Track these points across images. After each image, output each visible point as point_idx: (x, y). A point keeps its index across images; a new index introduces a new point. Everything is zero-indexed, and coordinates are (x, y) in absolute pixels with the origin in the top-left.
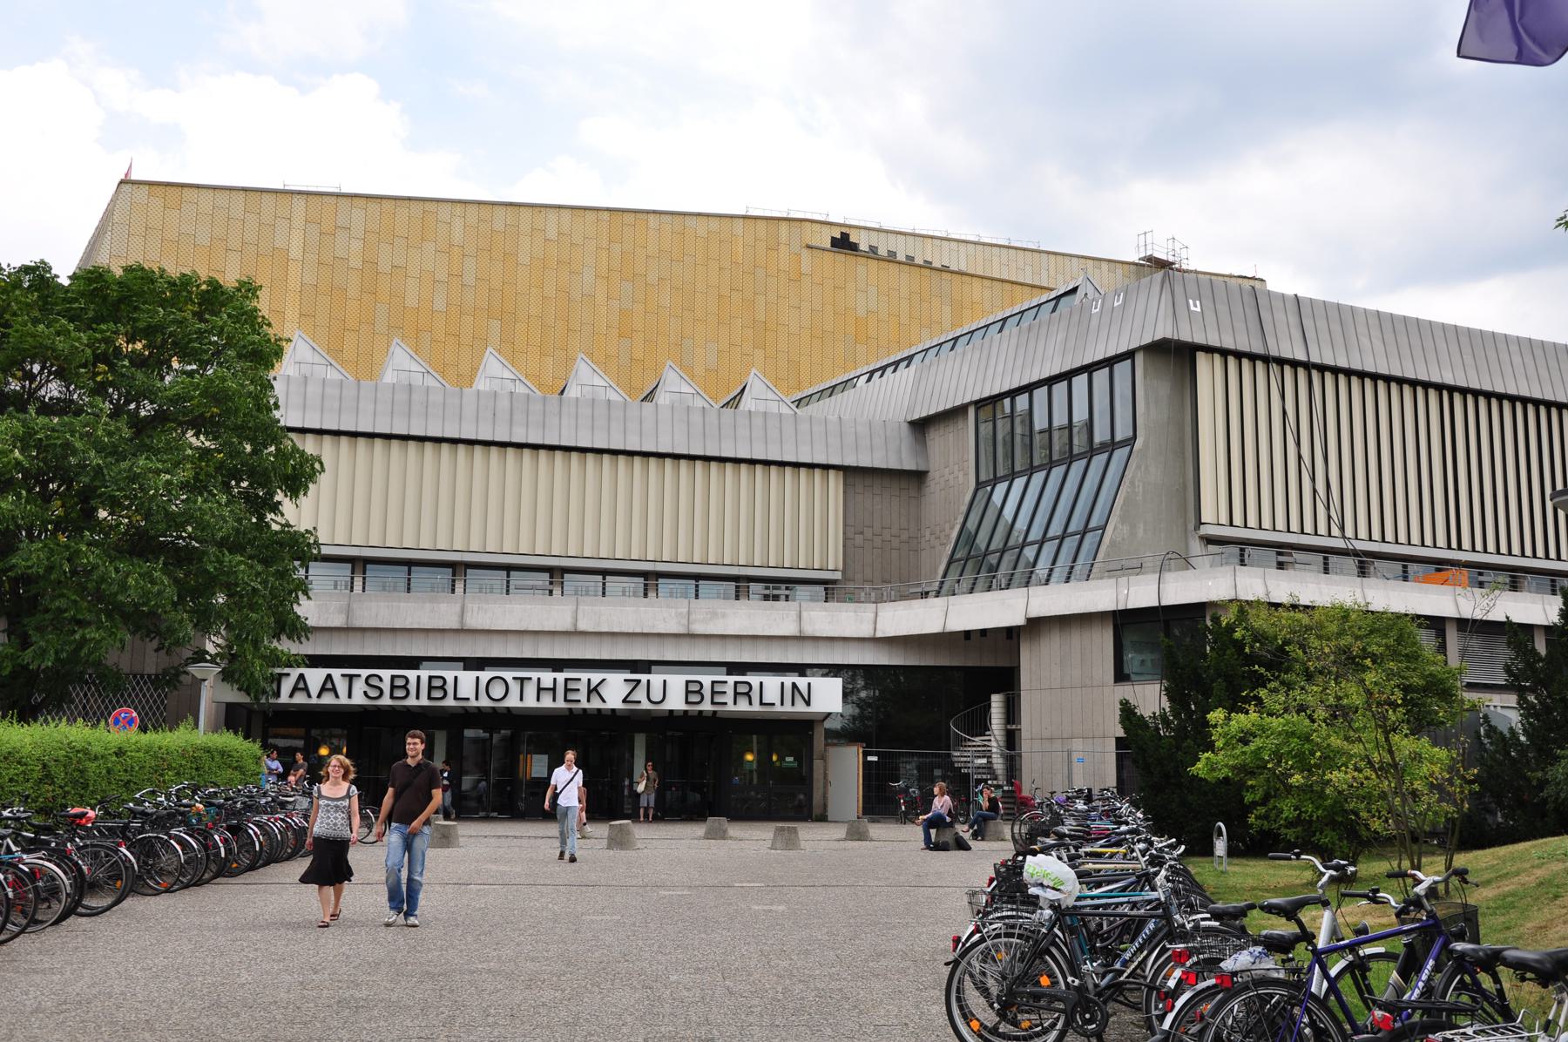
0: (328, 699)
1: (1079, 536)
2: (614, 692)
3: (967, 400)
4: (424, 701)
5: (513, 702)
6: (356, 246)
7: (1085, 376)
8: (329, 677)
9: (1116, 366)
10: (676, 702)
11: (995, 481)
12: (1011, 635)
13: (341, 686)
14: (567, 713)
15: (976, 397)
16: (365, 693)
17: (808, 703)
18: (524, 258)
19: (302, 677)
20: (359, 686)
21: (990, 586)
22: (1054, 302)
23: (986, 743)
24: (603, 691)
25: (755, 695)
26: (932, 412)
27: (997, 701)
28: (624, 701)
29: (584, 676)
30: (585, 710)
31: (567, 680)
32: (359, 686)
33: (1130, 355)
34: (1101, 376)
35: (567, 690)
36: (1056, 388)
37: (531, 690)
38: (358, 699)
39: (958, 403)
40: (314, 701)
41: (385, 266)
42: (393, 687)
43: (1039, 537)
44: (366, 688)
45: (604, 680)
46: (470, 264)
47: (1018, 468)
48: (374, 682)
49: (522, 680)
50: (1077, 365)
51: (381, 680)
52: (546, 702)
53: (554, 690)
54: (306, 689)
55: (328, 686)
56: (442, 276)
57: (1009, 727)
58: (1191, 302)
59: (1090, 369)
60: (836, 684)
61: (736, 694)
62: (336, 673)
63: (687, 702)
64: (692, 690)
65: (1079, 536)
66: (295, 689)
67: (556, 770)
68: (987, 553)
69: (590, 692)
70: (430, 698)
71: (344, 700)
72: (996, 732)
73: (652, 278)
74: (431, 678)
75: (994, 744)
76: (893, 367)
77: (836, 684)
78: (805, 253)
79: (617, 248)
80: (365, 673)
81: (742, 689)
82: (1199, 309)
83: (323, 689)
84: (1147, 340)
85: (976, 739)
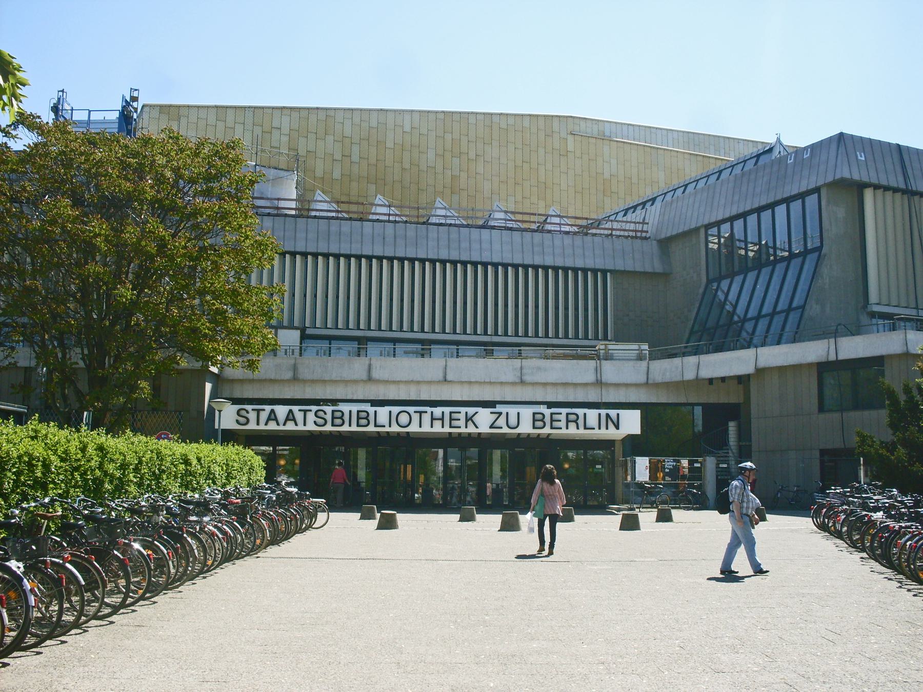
0: (290, 426)
1: (801, 310)
2: (484, 421)
3: (699, 225)
4: (354, 428)
5: (414, 428)
6: (285, 139)
7: (784, 206)
8: (291, 411)
9: (748, 217)
10: (526, 428)
11: (719, 279)
12: (742, 380)
13: (299, 416)
14: (448, 436)
15: (706, 222)
16: (315, 422)
17: (617, 427)
18: (390, 144)
19: (272, 411)
20: (311, 417)
21: (795, 340)
22: (756, 159)
23: (726, 454)
24: (475, 419)
25: (581, 421)
26: (674, 233)
27: (732, 426)
28: (491, 427)
29: (463, 410)
30: (388, 433)
31: (451, 413)
32: (311, 417)
33: (817, 190)
34: (796, 206)
35: (451, 419)
36: (763, 215)
37: (426, 418)
38: (311, 427)
39: (693, 226)
40: (281, 428)
41: (302, 152)
42: (333, 418)
43: (770, 311)
44: (325, 417)
45: (477, 413)
46: (356, 149)
47: (736, 269)
48: (321, 414)
49: (421, 413)
50: (779, 197)
51: (325, 413)
52: (437, 428)
53: (442, 419)
54: (276, 419)
55: (290, 417)
56: (338, 156)
57: (741, 444)
58: (858, 153)
59: (787, 201)
60: (637, 414)
61: (568, 421)
62: (295, 409)
63: (534, 428)
64: (537, 419)
65: (801, 310)
66: (269, 419)
67: (717, 511)
68: (745, 320)
69: (467, 421)
70: (358, 425)
71: (301, 427)
72: (732, 448)
73: (472, 155)
74: (358, 412)
75: (731, 454)
76: (651, 203)
77: (637, 414)
78: (570, 138)
79: (448, 137)
80: (314, 408)
81: (572, 417)
82: (863, 159)
83: (287, 419)
84: (830, 179)
85: (720, 452)
